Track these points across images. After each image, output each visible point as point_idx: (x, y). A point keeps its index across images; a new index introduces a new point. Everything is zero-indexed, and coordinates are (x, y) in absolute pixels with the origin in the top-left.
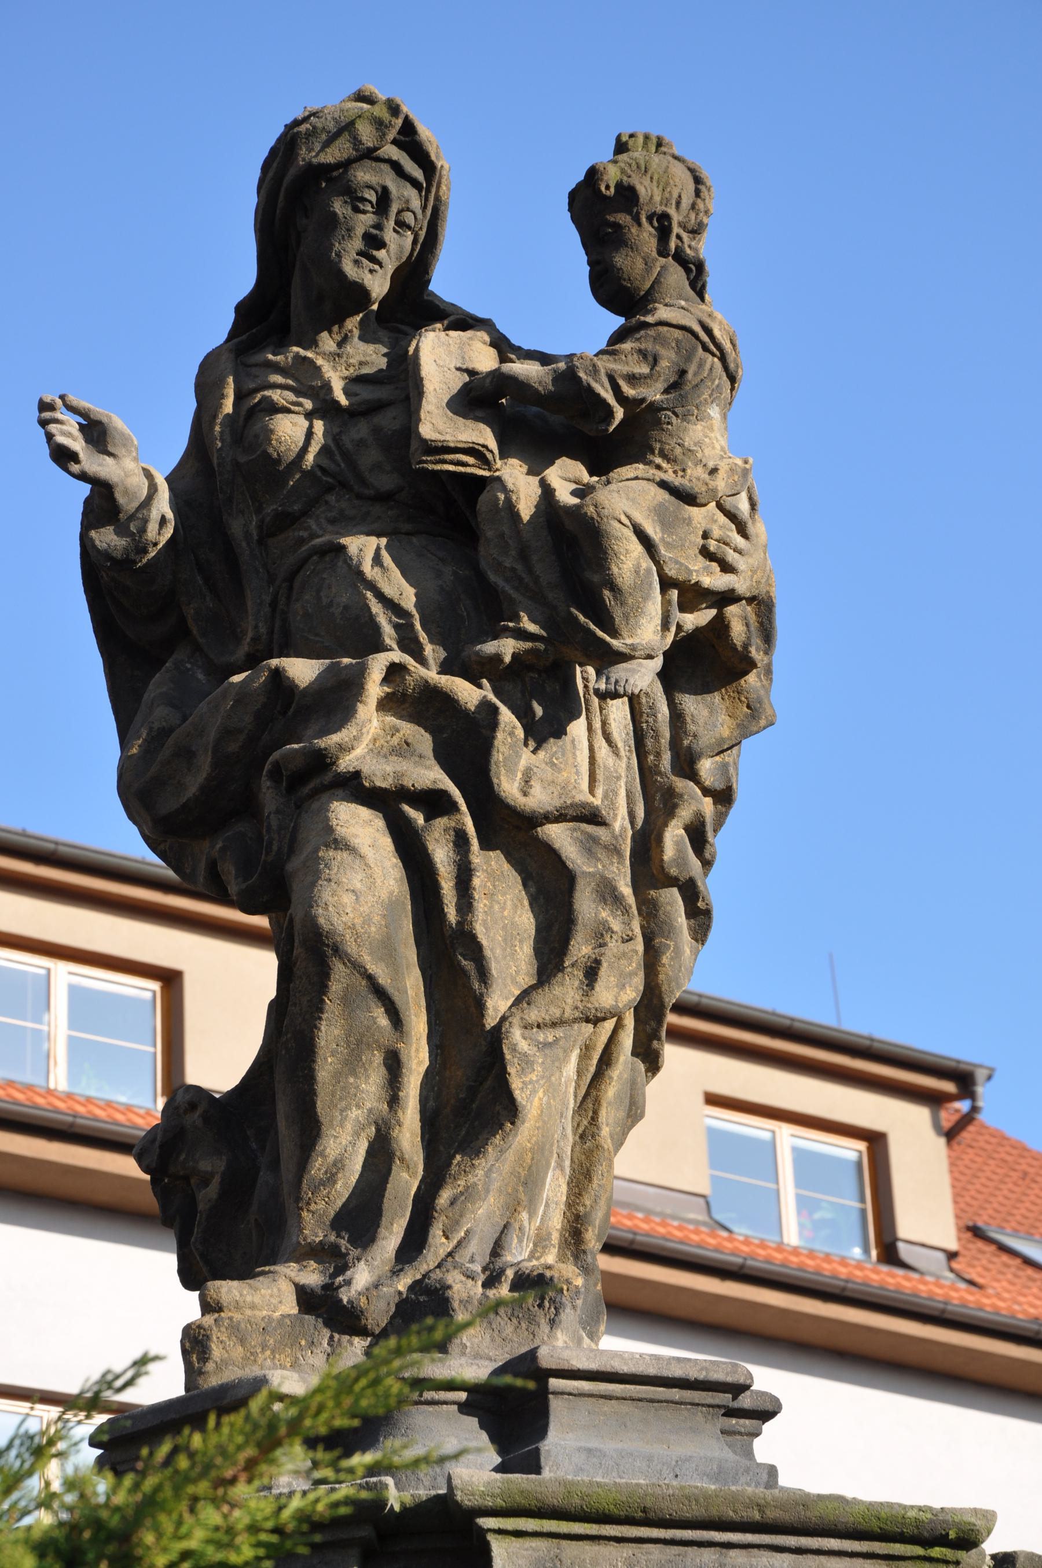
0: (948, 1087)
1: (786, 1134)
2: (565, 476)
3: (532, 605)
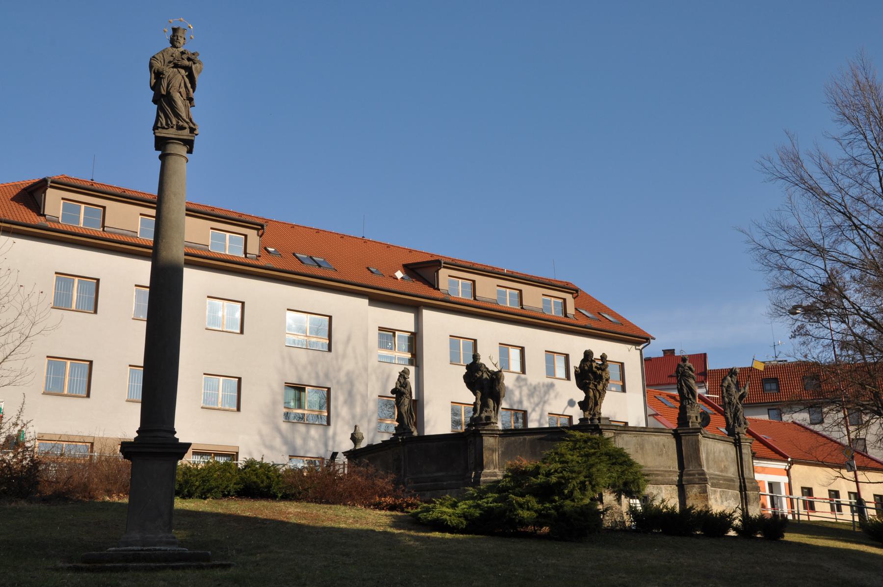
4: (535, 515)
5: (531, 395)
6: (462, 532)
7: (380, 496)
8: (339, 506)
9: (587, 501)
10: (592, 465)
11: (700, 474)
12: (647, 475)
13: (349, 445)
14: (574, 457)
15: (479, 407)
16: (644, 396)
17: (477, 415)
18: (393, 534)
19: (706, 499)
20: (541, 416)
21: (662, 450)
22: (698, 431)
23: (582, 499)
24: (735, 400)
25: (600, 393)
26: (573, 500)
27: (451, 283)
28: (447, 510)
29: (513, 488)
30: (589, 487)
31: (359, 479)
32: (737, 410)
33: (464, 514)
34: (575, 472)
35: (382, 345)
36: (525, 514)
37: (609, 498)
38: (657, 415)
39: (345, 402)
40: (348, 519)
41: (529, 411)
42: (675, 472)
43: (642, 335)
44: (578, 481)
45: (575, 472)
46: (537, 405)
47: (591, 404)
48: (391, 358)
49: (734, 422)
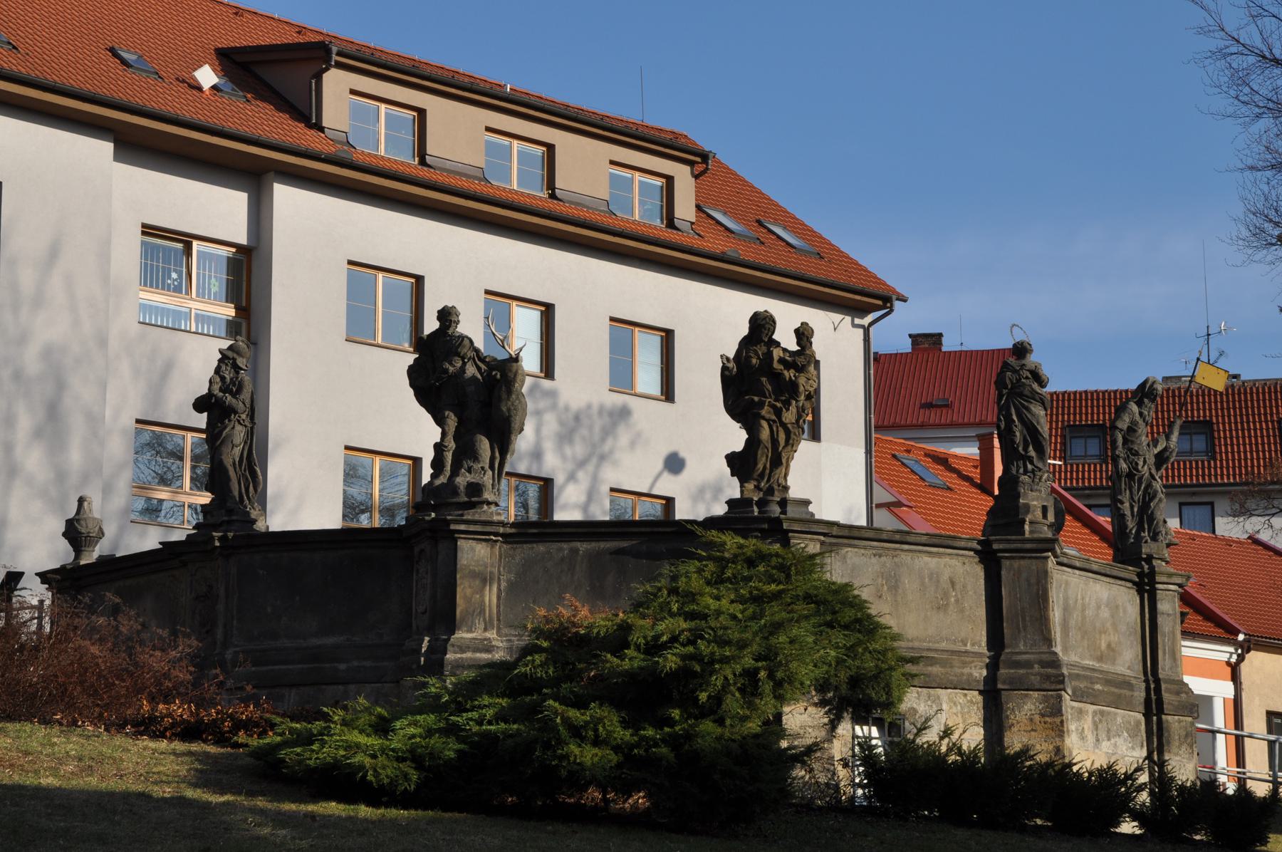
0: (699, 159)
1: (638, 176)
2: (792, 372)
3: (788, 391)
4: (614, 758)
5: (565, 437)
6: (405, 801)
7: (153, 699)
8: (28, 727)
9: (754, 726)
10: (777, 627)
11: (1044, 664)
12: (914, 661)
13: (55, 553)
14: (721, 604)
15: (449, 457)
16: (868, 452)
17: (442, 480)
18: (207, 806)
19: (1060, 731)
20: (591, 495)
21: (946, 595)
22: (1048, 545)
23: (744, 719)
24: (1145, 468)
25: (788, 433)
26: (720, 722)
27: (355, 113)
28: (363, 739)
29: (555, 682)
30: (767, 687)
31: (95, 650)
32: (1149, 495)
33: (412, 751)
34: (728, 643)
35: (152, 277)
36: (587, 755)
37: (801, 719)
38: (899, 504)
39: (38, 433)
40: (61, 762)
41: (559, 480)
42: (979, 655)
43: (872, 288)
44: (738, 669)
45: (728, 643)
46: (582, 464)
47: (762, 462)
48: (177, 315)
49: (1140, 528)
